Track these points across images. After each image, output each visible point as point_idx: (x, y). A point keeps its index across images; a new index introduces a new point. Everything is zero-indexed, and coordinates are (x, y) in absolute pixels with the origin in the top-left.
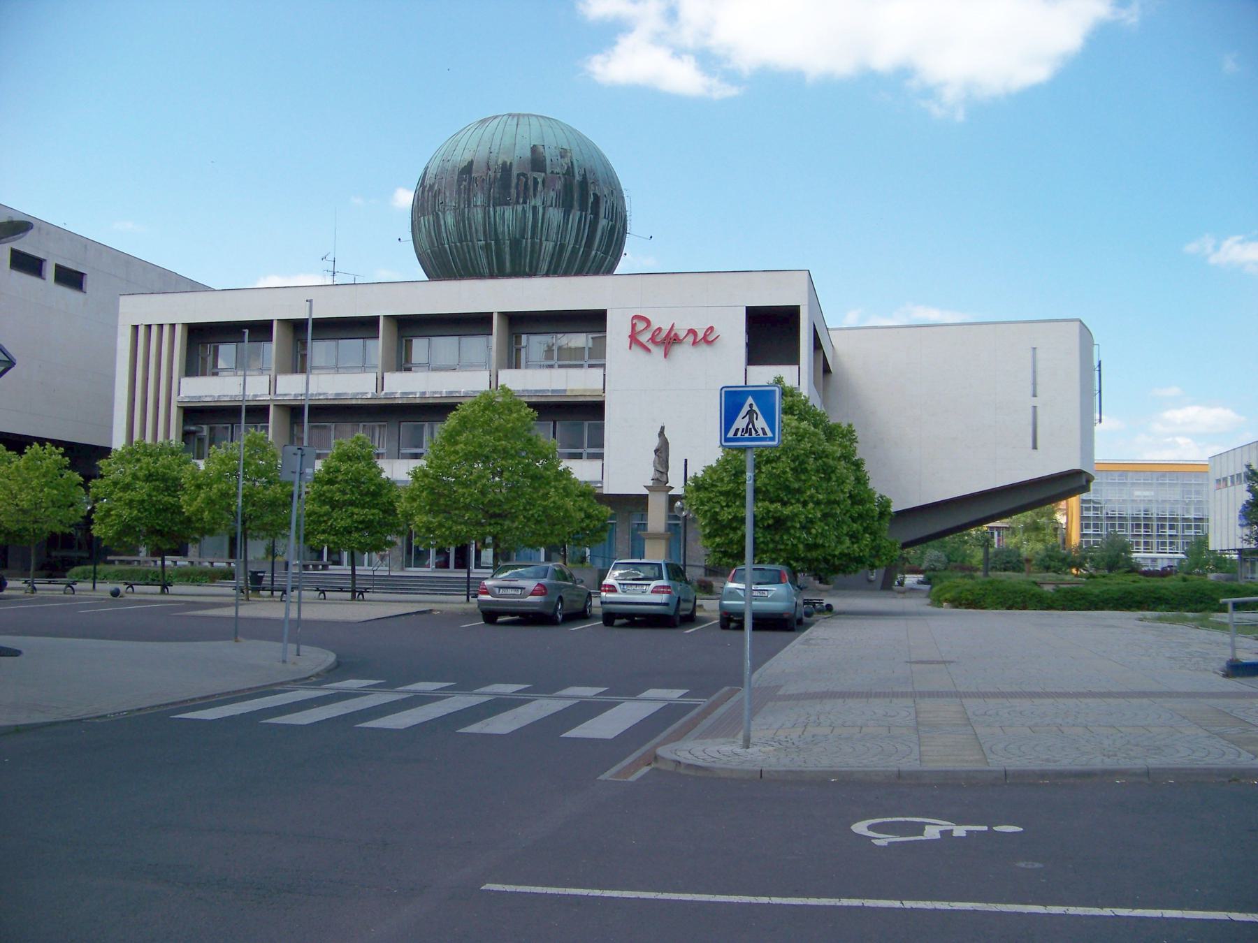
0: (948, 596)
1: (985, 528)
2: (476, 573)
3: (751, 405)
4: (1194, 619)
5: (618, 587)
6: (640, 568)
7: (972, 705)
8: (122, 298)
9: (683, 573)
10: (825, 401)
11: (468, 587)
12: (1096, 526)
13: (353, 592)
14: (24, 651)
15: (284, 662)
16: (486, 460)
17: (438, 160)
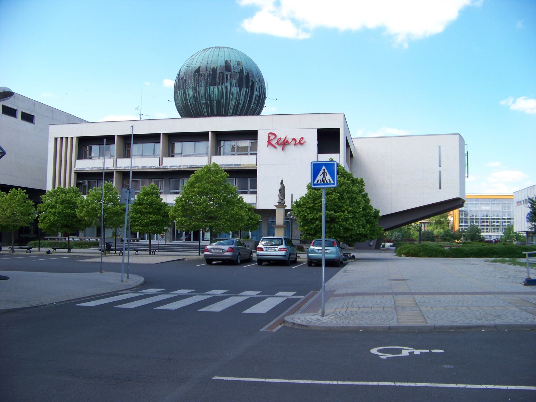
0: (404, 252)
1: (418, 223)
2: (202, 243)
3: (324, 170)
4: (509, 261)
5: (264, 249)
6: (273, 240)
7: (418, 298)
8: (50, 126)
9: (291, 241)
10: (351, 169)
11: (199, 249)
12: (465, 222)
13: (150, 251)
14: (10, 277)
15: (122, 281)
16: (207, 194)
17: (185, 67)
